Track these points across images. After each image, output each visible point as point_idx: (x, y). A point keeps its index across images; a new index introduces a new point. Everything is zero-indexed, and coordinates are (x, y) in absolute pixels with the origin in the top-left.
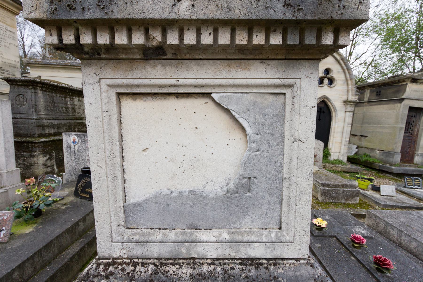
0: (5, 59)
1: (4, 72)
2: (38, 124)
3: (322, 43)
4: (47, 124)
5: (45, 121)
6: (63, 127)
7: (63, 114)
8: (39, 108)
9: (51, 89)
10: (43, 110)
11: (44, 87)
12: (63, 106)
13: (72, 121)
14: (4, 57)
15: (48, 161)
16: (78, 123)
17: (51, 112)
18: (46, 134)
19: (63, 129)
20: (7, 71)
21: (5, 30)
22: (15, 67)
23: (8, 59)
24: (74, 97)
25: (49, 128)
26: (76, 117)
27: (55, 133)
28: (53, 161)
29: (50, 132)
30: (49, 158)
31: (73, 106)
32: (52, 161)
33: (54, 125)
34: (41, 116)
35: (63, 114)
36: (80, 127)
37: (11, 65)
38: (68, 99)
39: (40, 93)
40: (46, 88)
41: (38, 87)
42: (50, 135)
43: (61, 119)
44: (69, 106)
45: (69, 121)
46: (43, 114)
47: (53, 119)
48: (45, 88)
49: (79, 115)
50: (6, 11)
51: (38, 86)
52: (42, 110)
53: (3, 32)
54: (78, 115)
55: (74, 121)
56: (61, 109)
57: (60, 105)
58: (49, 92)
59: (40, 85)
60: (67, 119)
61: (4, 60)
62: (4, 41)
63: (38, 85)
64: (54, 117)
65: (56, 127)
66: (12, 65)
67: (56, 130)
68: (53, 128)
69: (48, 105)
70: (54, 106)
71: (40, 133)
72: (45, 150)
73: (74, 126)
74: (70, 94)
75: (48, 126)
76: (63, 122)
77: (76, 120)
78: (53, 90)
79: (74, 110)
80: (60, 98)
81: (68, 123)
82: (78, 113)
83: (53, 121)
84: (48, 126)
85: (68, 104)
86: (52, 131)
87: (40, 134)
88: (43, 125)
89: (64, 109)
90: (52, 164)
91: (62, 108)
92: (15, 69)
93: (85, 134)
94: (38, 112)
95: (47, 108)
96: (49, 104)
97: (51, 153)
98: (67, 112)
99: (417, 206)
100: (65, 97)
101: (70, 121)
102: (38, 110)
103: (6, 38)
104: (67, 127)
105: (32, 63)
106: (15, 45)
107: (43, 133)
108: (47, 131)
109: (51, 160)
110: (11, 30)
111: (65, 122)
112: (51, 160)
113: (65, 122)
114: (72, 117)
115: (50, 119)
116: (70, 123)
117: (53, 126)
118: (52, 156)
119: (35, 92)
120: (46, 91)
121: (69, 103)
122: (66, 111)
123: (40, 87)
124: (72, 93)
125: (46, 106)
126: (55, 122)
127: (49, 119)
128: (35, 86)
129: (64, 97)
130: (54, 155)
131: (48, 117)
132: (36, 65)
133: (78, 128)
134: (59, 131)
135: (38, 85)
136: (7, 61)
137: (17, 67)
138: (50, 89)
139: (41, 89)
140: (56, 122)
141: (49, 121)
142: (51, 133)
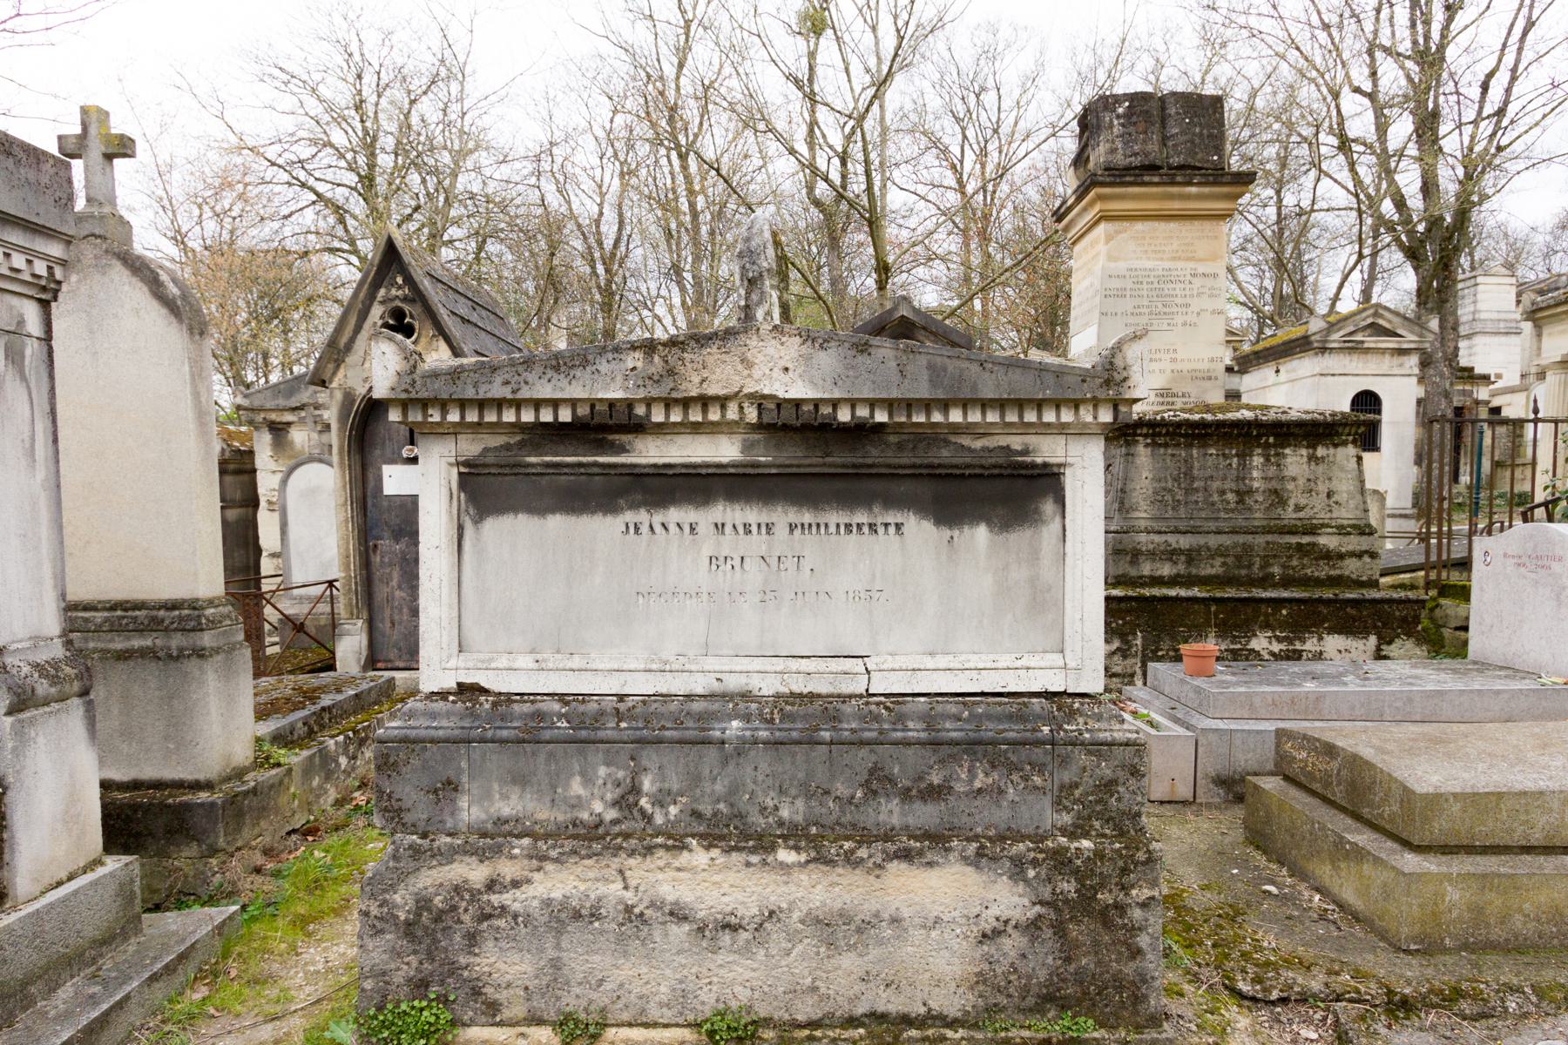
0: (1182, 360)
1: (1175, 399)
2: (1120, 547)
3: (385, 468)
4: (1151, 547)
5: (1143, 537)
6: (1212, 557)
7: (1222, 515)
8: (1134, 501)
9: (1186, 436)
10: (1143, 505)
11: (1160, 435)
12: (1229, 485)
13: (1260, 540)
14: (1179, 356)
15: (1116, 658)
16: (1289, 546)
17: (1173, 509)
18: (1141, 577)
19: (1212, 566)
20: (1183, 396)
21: (1189, 277)
22: (1210, 378)
23: (1189, 360)
24: (1287, 451)
25: (1154, 560)
26: (1286, 522)
27: (1178, 575)
28: (1133, 661)
29: (1158, 573)
30: (1118, 649)
31: (1274, 484)
32: (1130, 661)
33: (1175, 549)
34: (1136, 523)
35: (1222, 515)
36: (1295, 563)
37: (1198, 374)
38: (1257, 460)
39: (1142, 452)
40: (1168, 434)
41: (1141, 438)
42: (1157, 581)
43: (1208, 533)
44: (1256, 485)
45: (1241, 539)
46: (1144, 515)
47: (1177, 531)
48: (1165, 435)
49: (1301, 515)
50: (1196, 223)
51: (1140, 435)
52: (1142, 503)
53: (1182, 286)
54: (1294, 516)
55: (1269, 538)
56: (1216, 498)
57: (1216, 485)
58: (1178, 445)
59: (1145, 431)
60: (1234, 532)
61: (1179, 366)
62: (1184, 310)
63: (1139, 431)
64: (1182, 526)
65: (1183, 558)
66: (1201, 375)
67: (1181, 568)
68: (1171, 560)
69: (1165, 489)
70: (1189, 491)
71: (1120, 573)
72: (1114, 625)
73: (1266, 556)
74: (1271, 440)
75: (1152, 555)
76: (1213, 541)
77: (1281, 533)
78: (1194, 436)
79: (1278, 497)
80: (1221, 458)
81: (1236, 545)
82: (1298, 508)
83: (1172, 539)
84: (1152, 555)
85: (1252, 479)
86: (1166, 570)
87: (1123, 575)
88: (1135, 549)
89: (1230, 497)
90: (1129, 671)
91: (1222, 493)
92: (1208, 384)
93: (1124, 568)
94: (1127, 512)
95: (1158, 500)
96: (1170, 485)
97: (1127, 634)
98: (1241, 506)
99: (346, 521)
100: (1242, 456)
101: (1249, 538)
102: (1127, 506)
103: (1188, 300)
104: (1230, 560)
105: (1544, 305)
106: (1213, 312)
107: (1133, 572)
108: (1146, 569)
109: (1125, 657)
110: (1207, 272)
111: (1227, 540)
112: (1125, 657)
113: (1227, 540)
114: (1265, 523)
115: (1166, 533)
116: (1247, 548)
117: (1171, 554)
118: (1130, 647)
119: (1128, 454)
120: (1166, 445)
121: (1255, 474)
122: (1241, 501)
123: (1146, 436)
124: (1276, 436)
125: (1156, 493)
126: (1181, 542)
127: (1160, 532)
128: (1129, 435)
129: (1237, 455)
130: (1139, 642)
131: (1156, 525)
132: (1559, 310)
133: (1284, 566)
134: (1194, 571)
135: (1139, 431)
136: (1187, 366)
137: (1213, 375)
138: (1181, 435)
139: (1149, 441)
140: (1184, 542)
141: (1157, 538)
142: (1162, 577)
